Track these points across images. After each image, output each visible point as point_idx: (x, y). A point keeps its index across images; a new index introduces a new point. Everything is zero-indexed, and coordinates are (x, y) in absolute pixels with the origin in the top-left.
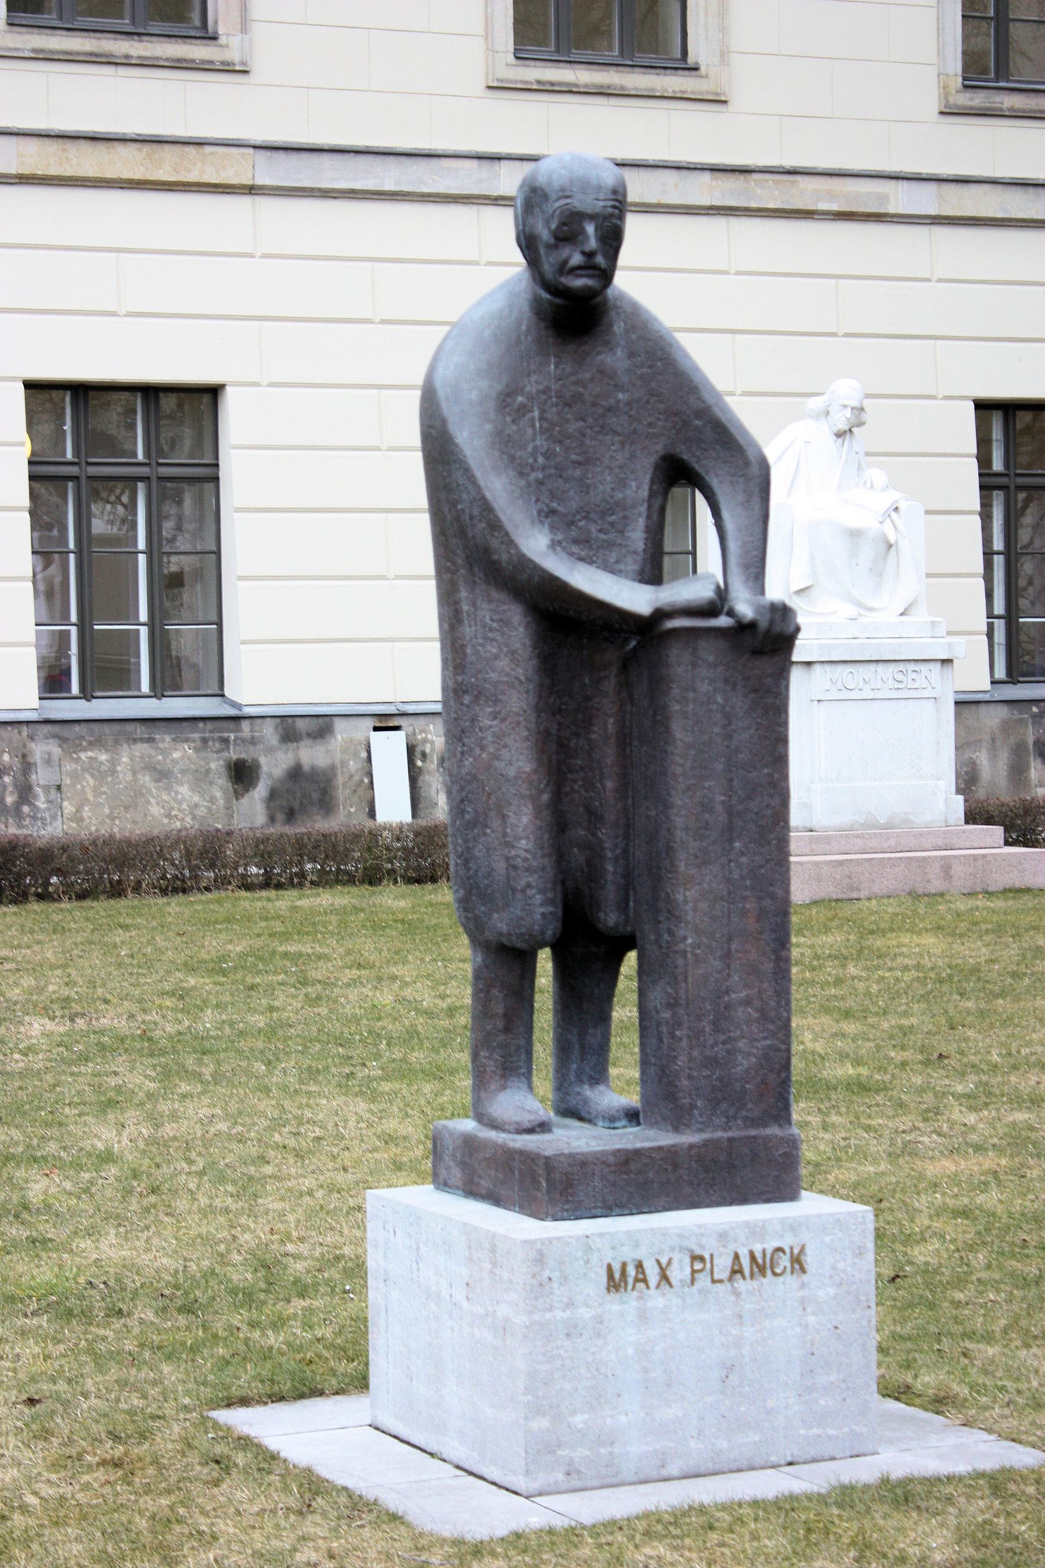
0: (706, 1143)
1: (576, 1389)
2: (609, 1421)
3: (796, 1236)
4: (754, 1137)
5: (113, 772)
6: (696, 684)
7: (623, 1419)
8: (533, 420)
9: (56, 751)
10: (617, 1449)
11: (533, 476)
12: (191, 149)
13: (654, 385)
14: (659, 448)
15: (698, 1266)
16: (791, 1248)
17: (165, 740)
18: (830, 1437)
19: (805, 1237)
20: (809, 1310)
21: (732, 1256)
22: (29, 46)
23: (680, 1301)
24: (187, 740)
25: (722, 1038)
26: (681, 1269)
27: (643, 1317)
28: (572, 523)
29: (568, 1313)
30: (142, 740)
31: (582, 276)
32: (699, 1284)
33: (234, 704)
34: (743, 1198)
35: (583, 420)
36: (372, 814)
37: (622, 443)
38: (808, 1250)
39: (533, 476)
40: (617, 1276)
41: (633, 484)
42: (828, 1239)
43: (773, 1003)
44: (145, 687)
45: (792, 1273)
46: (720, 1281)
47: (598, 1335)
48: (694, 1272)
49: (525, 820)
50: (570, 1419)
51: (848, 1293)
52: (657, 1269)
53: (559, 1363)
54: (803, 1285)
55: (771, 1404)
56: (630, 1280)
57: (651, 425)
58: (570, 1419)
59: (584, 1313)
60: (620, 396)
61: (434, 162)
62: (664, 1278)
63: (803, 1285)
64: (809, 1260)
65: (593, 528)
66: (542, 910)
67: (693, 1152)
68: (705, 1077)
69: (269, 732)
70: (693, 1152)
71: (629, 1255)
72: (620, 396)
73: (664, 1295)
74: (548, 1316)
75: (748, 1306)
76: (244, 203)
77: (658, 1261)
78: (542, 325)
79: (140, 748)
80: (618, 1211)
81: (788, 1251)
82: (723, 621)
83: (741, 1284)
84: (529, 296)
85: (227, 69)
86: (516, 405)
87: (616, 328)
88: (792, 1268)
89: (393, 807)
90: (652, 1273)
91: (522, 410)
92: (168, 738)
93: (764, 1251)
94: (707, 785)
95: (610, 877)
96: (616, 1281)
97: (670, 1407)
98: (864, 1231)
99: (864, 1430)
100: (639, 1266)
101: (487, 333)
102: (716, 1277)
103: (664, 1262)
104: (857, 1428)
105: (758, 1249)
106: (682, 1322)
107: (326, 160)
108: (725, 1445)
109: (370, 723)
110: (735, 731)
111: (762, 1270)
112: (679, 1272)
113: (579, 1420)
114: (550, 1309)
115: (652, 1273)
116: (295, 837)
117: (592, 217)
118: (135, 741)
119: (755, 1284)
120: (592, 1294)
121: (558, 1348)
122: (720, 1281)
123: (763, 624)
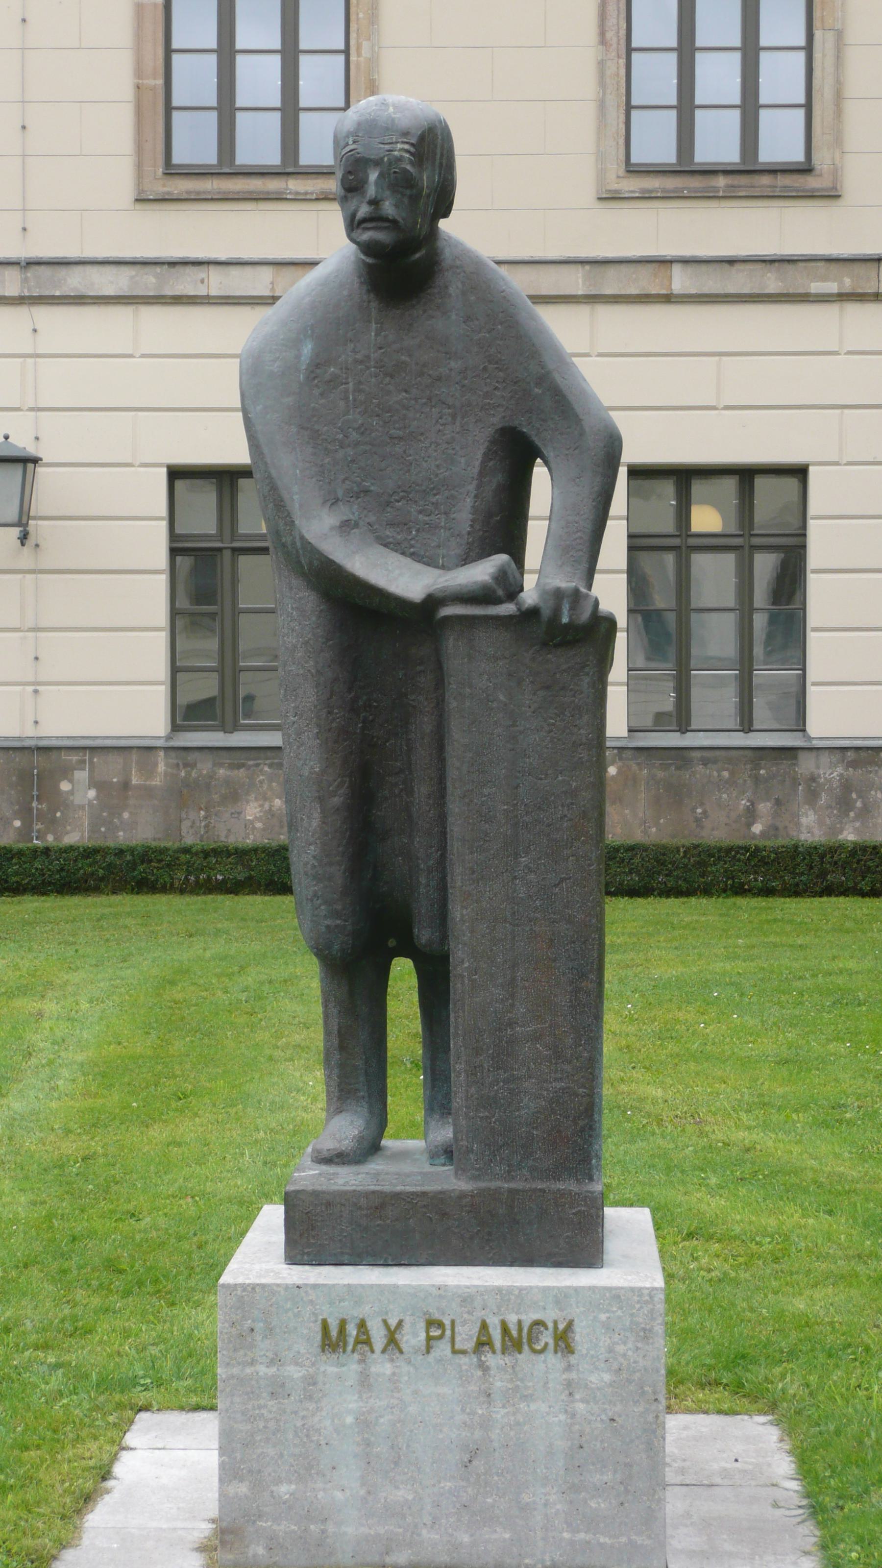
0: (482, 1192)
1: (281, 1455)
2: (321, 1495)
3: (561, 1310)
4: (543, 1191)
7: (339, 1495)
8: (346, 391)
10: (331, 1529)
11: (341, 454)
13: (493, 350)
14: (496, 420)
15: (435, 1333)
16: (555, 1323)
18: (602, 1546)
19: (575, 1311)
20: (577, 1397)
21: (479, 1324)
25: (504, 1075)
26: (415, 1335)
27: (365, 1382)
28: (388, 504)
31: (368, 229)
32: (435, 1353)
34: (528, 1260)
35: (406, 391)
37: (454, 416)
38: (578, 1328)
39: (341, 454)
40: (334, 1333)
41: (463, 460)
42: (603, 1317)
43: (569, 1041)
45: (556, 1352)
46: (464, 1352)
47: (310, 1398)
48: (429, 1338)
49: (315, 823)
50: (274, 1488)
51: (629, 1381)
52: (383, 1332)
53: (261, 1425)
54: (569, 1368)
55: (526, 1498)
56: (351, 1341)
57: (487, 395)
58: (274, 1488)
59: (295, 1372)
60: (453, 364)
62: (392, 1342)
63: (569, 1368)
64: (580, 1336)
65: (413, 509)
66: (328, 922)
67: (464, 1201)
68: (481, 1118)
70: (464, 1201)
71: (354, 1313)
72: (453, 364)
73: (392, 1360)
74: (249, 1370)
75: (498, 1384)
77: (385, 1322)
78: (365, 287)
80: (370, 1260)
81: (550, 1325)
82: (507, 609)
83: (492, 1360)
84: (353, 258)
86: (327, 377)
87: (452, 290)
88: (556, 1345)
90: (378, 1337)
91: (333, 382)
93: (520, 1322)
94: (486, 791)
95: (422, 890)
96: (333, 1340)
97: (397, 1488)
98: (652, 1311)
99: (647, 1542)
100: (362, 1325)
101: (307, 299)
102: (457, 1347)
103: (393, 1322)
104: (639, 1540)
105: (512, 1319)
106: (430, 1396)
108: (466, 1539)
110: (521, 733)
111: (517, 1346)
112: (413, 1337)
113: (284, 1490)
114: (252, 1363)
115: (378, 1337)
117: (377, 163)
119: (508, 1359)
120: (303, 1351)
121: (260, 1407)
122: (464, 1352)
123: (546, 613)
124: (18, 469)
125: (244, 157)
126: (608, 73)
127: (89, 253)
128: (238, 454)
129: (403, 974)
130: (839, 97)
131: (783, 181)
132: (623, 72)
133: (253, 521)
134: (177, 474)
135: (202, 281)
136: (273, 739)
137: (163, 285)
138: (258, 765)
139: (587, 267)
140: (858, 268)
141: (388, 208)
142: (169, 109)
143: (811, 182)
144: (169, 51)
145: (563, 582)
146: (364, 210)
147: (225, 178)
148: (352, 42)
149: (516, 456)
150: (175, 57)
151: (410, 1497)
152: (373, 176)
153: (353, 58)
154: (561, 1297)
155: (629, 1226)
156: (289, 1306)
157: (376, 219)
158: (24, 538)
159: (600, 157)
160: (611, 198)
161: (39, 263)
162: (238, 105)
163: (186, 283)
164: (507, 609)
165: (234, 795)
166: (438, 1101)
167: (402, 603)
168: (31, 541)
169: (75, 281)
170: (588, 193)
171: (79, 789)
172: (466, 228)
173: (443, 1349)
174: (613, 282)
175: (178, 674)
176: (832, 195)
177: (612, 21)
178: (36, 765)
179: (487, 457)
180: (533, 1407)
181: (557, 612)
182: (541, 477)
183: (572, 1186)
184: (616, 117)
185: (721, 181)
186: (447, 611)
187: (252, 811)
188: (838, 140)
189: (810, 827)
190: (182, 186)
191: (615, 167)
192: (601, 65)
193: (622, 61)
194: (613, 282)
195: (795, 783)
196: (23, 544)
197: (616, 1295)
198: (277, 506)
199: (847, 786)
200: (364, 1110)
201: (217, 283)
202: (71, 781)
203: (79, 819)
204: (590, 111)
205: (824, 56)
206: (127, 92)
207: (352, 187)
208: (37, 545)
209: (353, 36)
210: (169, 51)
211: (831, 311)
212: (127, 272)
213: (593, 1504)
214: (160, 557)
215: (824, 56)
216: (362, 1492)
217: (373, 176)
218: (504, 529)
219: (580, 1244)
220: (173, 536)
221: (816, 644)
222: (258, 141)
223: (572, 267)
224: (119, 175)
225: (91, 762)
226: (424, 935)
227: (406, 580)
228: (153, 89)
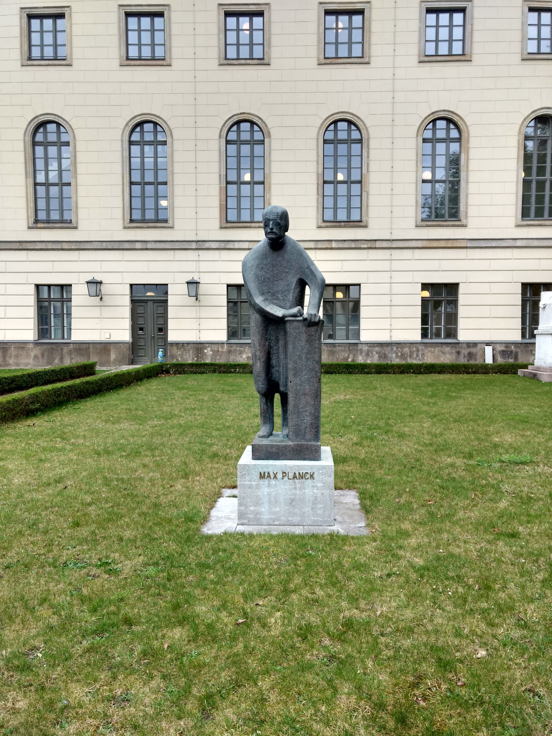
14: (298, 277)
17: (444, 346)
34: (305, 459)
59: (254, 483)
62: (275, 477)
64: (315, 476)
69: (465, 345)
71: (266, 470)
76: (465, 250)
79: (440, 348)
82: (301, 318)
85: (463, 226)
89: (489, 360)
90: (272, 476)
96: (262, 476)
100: (269, 473)
105: (301, 472)
106: (283, 488)
107: (481, 241)
112: (280, 476)
113: (252, 508)
115: (272, 476)
116: (197, 365)
123: (309, 319)
125: (243, 219)
128: (242, 282)
129: (277, 396)
130: (367, 206)
131: (356, 224)
133: (244, 297)
134: (228, 286)
136: (249, 341)
137: (225, 246)
141: (274, 230)
143: (362, 224)
144: (227, 196)
145: (313, 312)
146: (269, 230)
147: (240, 224)
149: (302, 284)
152: (271, 223)
154: (312, 467)
155: (326, 451)
157: (272, 232)
158: (197, 299)
159: (317, 219)
160: (319, 227)
162: (454, 38)
163: (230, 245)
164: (301, 318)
165: (241, 353)
167: (278, 317)
170: (315, 226)
171: (208, 352)
172: (291, 234)
173: (286, 478)
174: (320, 245)
176: (366, 227)
179: (296, 284)
181: (311, 319)
182: (307, 290)
183: (313, 443)
185: (343, 224)
186: (286, 319)
187: (244, 356)
189: (360, 360)
190: (328, 61)
191: (320, 221)
192: (318, 199)
194: (320, 245)
195: (358, 350)
197: (324, 467)
198: (249, 294)
199: (368, 351)
200: (269, 426)
201: (237, 245)
203: (208, 357)
204: (315, 209)
206: (218, 205)
207: (266, 226)
211: (366, 251)
212: (218, 243)
214: (225, 303)
217: (271, 223)
218: (300, 302)
219: (315, 455)
220: (228, 299)
221: (362, 321)
222: (245, 216)
224: (216, 223)
226: (282, 389)
227: (278, 312)
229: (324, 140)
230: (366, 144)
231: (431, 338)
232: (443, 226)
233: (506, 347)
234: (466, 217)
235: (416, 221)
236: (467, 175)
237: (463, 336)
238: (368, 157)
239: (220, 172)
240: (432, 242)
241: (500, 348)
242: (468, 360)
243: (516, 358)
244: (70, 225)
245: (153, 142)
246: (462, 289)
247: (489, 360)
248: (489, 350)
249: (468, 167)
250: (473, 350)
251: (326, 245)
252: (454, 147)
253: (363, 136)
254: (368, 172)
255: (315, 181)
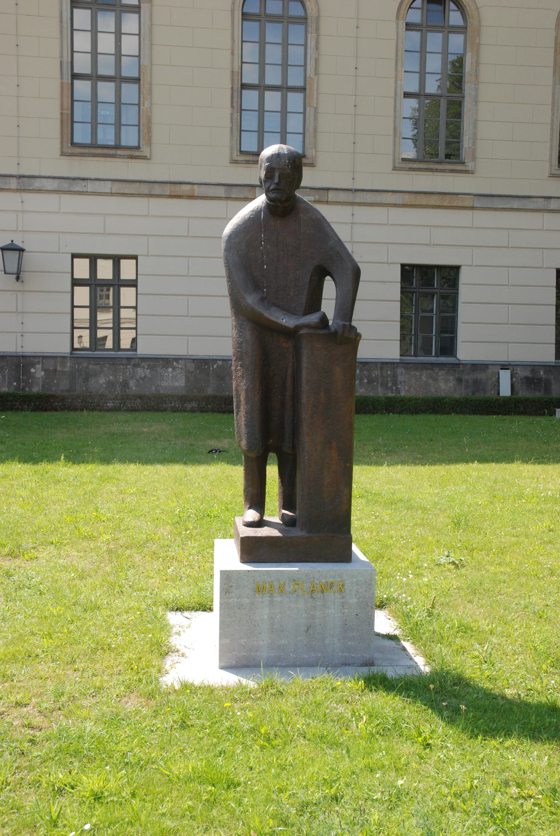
5: (421, 378)
6: (311, 357)
7: (262, 642)
9: (404, 371)
12: (455, 196)
22: (408, 167)
23: (288, 599)
24: (443, 370)
29: (239, 600)
30: (430, 369)
33: (459, 360)
36: (499, 394)
44: (433, 354)
59: (246, 601)
61: (530, 199)
85: (467, 172)
89: (505, 390)
92: (437, 369)
96: (259, 590)
107: (496, 199)
108: (306, 656)
109: (500, 367)
118: (428, 369)
123: (340, 332)
124: (18, 253)
126: (234, 118)
127: (43, 174)
130: (315, 131)
132: (239, 118)
135: (85, 186)
138: (104, 364)
139: (226, 187)
140: (321, 192)
142: (73, 122)
144: (73, 101)
148: (141, 101)
150: (75, 103)
151: (287, 643)
153: (142, 107)
156: (245, 577)
158: (18, 279)
159: (232, 148)
160: (234, 162)
161: (24, 176)
166: (288, 501)
168: (21, 279)
169: (37, 184)
175: (75, 330)
177: (235, 99)
178: (20, 363)
180: (330, 611)
184: (236, 133)
188: (315, 146)
190: (78, 150)
191: (236, 153)
193: (239, 114)
196: (17, 281)
202: (35, 369)
204: (228, 131)
205: (310, 116)
208: (23, 281)
209: (142, 99)
210: (73, 101)
212: (57, 181)
213: (349, 643)
215: (310, 116)
216: (270, 641)
218: (314, 302)
223: (220, 187)
225: (42, 362)
227: (287, 321)
228: (67, 114)
229: (243, 14)
230: (314, 26)
231: (416, 355)
232: (437, 170)
233: (533, 371)
234: (474, 159)
235: (394, 161)
236: (477, 90)
237: (465, 352)
238: (317, 48)
239: (62, 56)
240: (419, 196)
241: (522, 373)
242: (473, 393)
243: (548, 389)
244: (136, 153)
245: (259, 16)
246: (464, 277)
247: (505, 390)
248: (505, 377)
249: (477, 77)
250: (481, 376)
251: (541, 203)
252: (456, 42)
253: (309, 12)
254: (317, 73)
255: (228, 84)
